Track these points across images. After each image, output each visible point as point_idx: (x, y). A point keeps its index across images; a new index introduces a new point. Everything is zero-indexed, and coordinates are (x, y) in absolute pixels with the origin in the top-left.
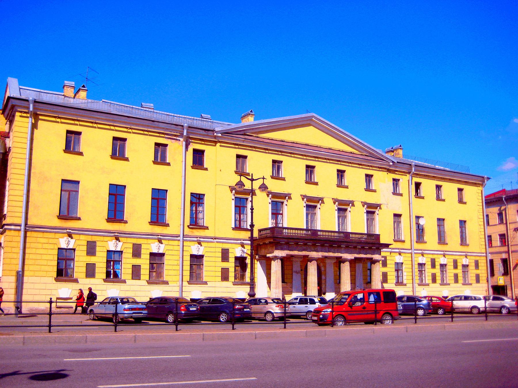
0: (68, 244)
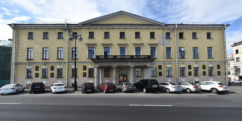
0: (60, 67)
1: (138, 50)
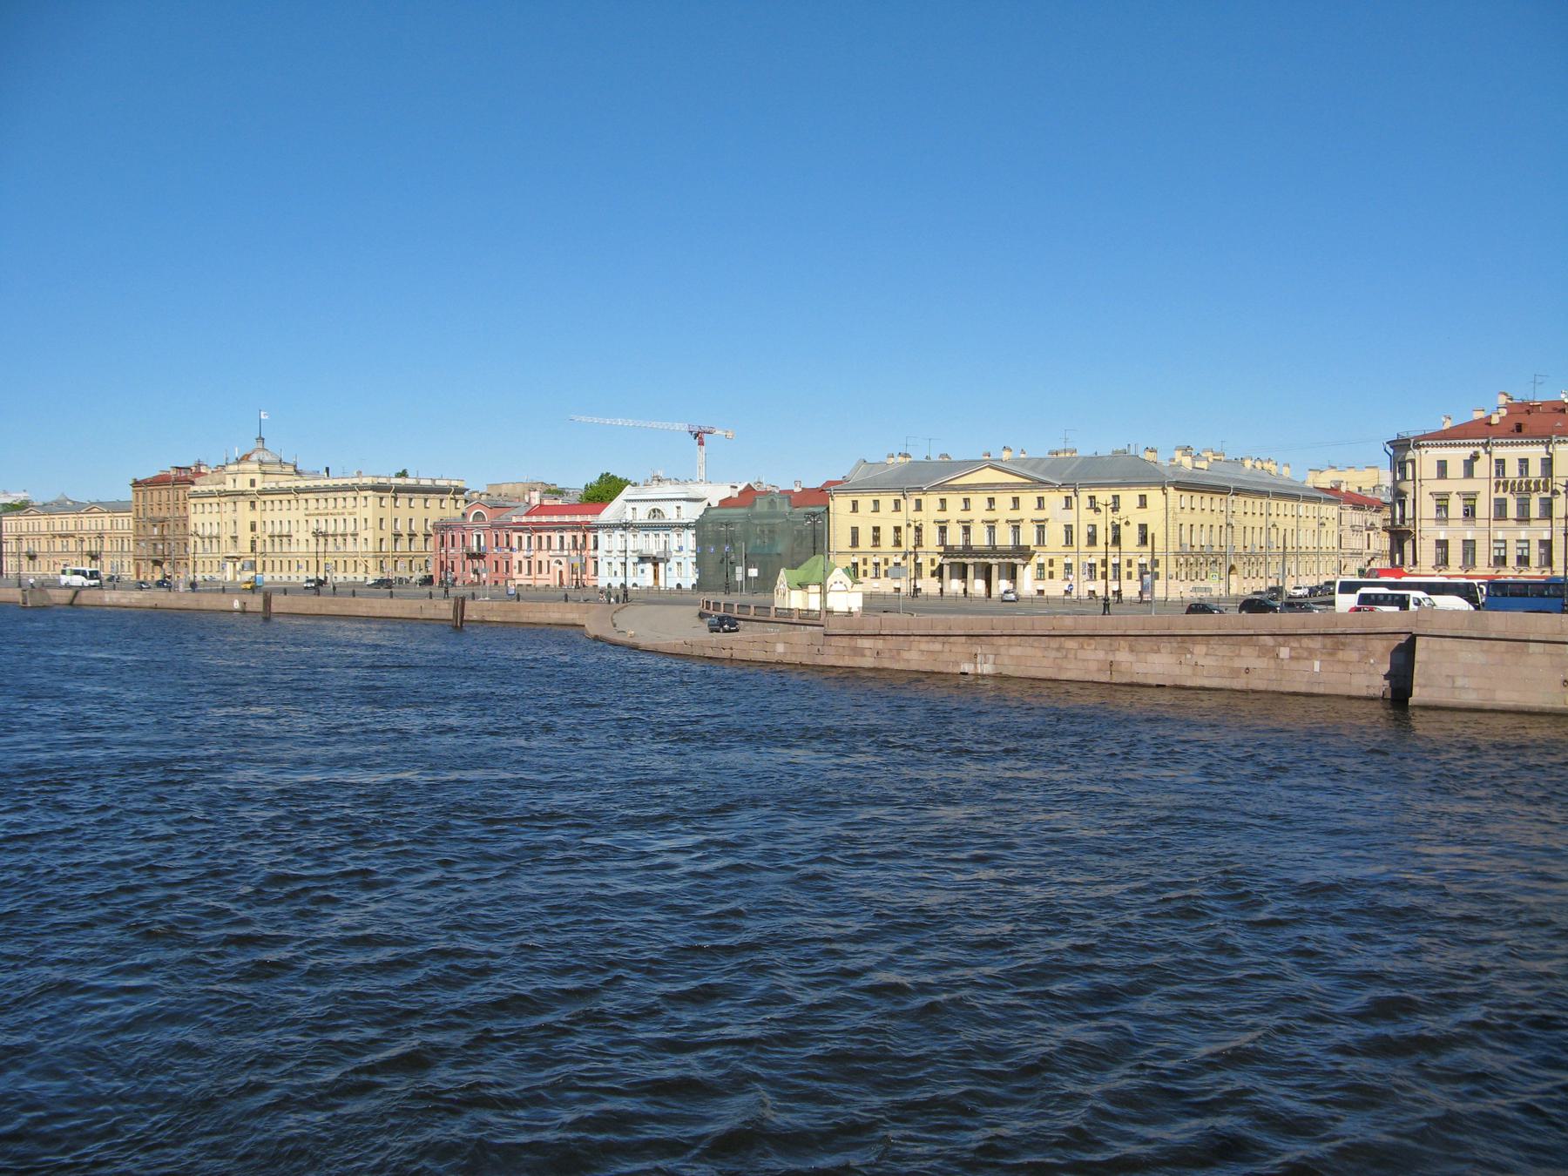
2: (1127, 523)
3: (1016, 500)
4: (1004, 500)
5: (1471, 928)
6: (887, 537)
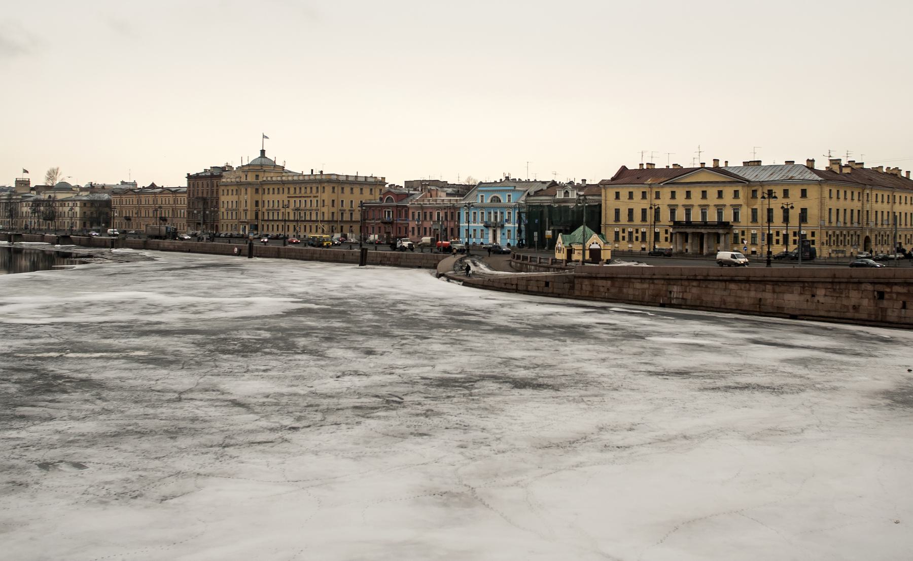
1: (688, 214)
2: (792, 207)
3: (704, 193)
4: (712, 192)
5: (162, 372)
6: (638, 215)
